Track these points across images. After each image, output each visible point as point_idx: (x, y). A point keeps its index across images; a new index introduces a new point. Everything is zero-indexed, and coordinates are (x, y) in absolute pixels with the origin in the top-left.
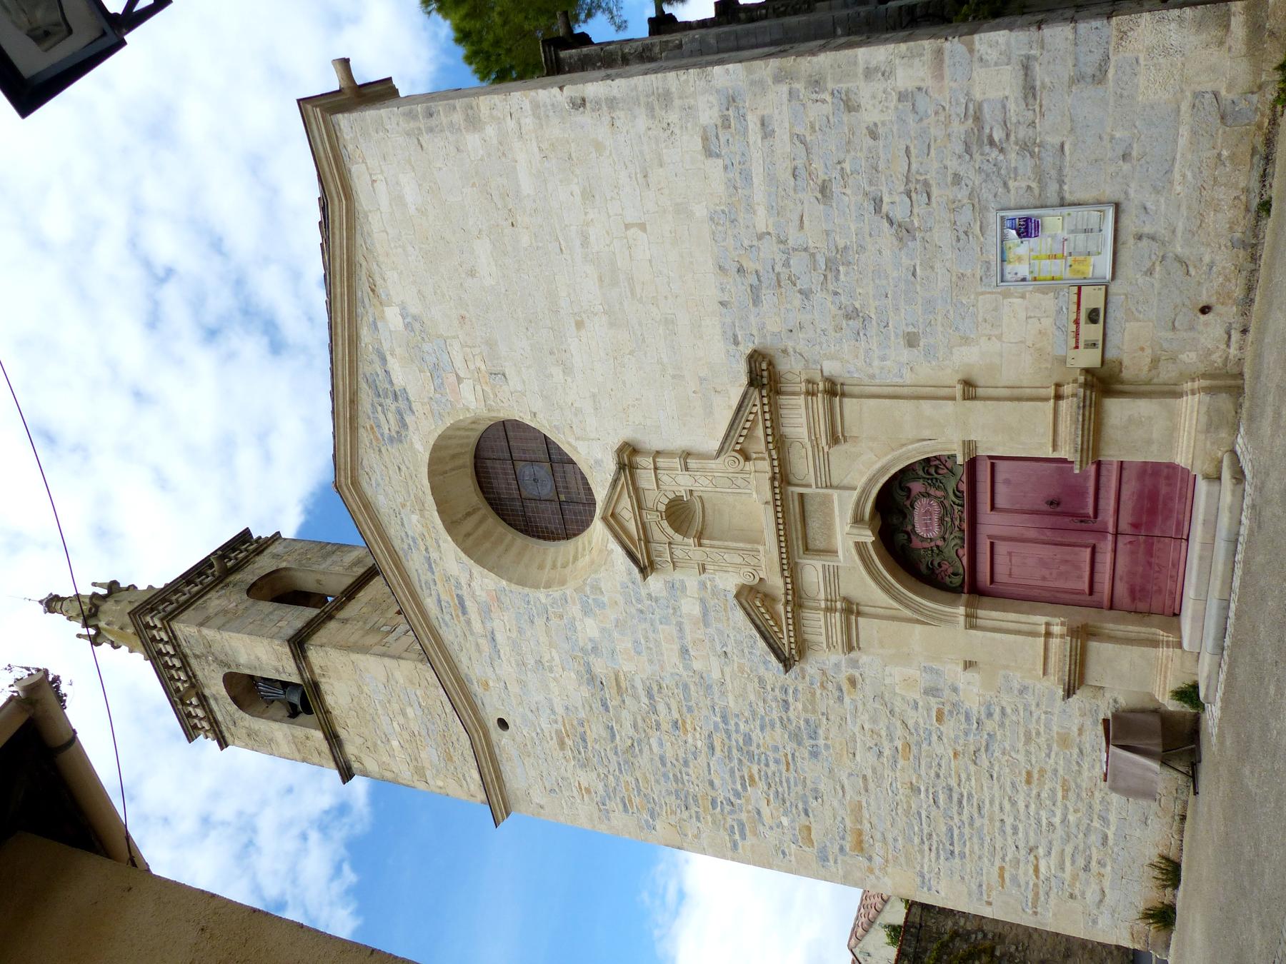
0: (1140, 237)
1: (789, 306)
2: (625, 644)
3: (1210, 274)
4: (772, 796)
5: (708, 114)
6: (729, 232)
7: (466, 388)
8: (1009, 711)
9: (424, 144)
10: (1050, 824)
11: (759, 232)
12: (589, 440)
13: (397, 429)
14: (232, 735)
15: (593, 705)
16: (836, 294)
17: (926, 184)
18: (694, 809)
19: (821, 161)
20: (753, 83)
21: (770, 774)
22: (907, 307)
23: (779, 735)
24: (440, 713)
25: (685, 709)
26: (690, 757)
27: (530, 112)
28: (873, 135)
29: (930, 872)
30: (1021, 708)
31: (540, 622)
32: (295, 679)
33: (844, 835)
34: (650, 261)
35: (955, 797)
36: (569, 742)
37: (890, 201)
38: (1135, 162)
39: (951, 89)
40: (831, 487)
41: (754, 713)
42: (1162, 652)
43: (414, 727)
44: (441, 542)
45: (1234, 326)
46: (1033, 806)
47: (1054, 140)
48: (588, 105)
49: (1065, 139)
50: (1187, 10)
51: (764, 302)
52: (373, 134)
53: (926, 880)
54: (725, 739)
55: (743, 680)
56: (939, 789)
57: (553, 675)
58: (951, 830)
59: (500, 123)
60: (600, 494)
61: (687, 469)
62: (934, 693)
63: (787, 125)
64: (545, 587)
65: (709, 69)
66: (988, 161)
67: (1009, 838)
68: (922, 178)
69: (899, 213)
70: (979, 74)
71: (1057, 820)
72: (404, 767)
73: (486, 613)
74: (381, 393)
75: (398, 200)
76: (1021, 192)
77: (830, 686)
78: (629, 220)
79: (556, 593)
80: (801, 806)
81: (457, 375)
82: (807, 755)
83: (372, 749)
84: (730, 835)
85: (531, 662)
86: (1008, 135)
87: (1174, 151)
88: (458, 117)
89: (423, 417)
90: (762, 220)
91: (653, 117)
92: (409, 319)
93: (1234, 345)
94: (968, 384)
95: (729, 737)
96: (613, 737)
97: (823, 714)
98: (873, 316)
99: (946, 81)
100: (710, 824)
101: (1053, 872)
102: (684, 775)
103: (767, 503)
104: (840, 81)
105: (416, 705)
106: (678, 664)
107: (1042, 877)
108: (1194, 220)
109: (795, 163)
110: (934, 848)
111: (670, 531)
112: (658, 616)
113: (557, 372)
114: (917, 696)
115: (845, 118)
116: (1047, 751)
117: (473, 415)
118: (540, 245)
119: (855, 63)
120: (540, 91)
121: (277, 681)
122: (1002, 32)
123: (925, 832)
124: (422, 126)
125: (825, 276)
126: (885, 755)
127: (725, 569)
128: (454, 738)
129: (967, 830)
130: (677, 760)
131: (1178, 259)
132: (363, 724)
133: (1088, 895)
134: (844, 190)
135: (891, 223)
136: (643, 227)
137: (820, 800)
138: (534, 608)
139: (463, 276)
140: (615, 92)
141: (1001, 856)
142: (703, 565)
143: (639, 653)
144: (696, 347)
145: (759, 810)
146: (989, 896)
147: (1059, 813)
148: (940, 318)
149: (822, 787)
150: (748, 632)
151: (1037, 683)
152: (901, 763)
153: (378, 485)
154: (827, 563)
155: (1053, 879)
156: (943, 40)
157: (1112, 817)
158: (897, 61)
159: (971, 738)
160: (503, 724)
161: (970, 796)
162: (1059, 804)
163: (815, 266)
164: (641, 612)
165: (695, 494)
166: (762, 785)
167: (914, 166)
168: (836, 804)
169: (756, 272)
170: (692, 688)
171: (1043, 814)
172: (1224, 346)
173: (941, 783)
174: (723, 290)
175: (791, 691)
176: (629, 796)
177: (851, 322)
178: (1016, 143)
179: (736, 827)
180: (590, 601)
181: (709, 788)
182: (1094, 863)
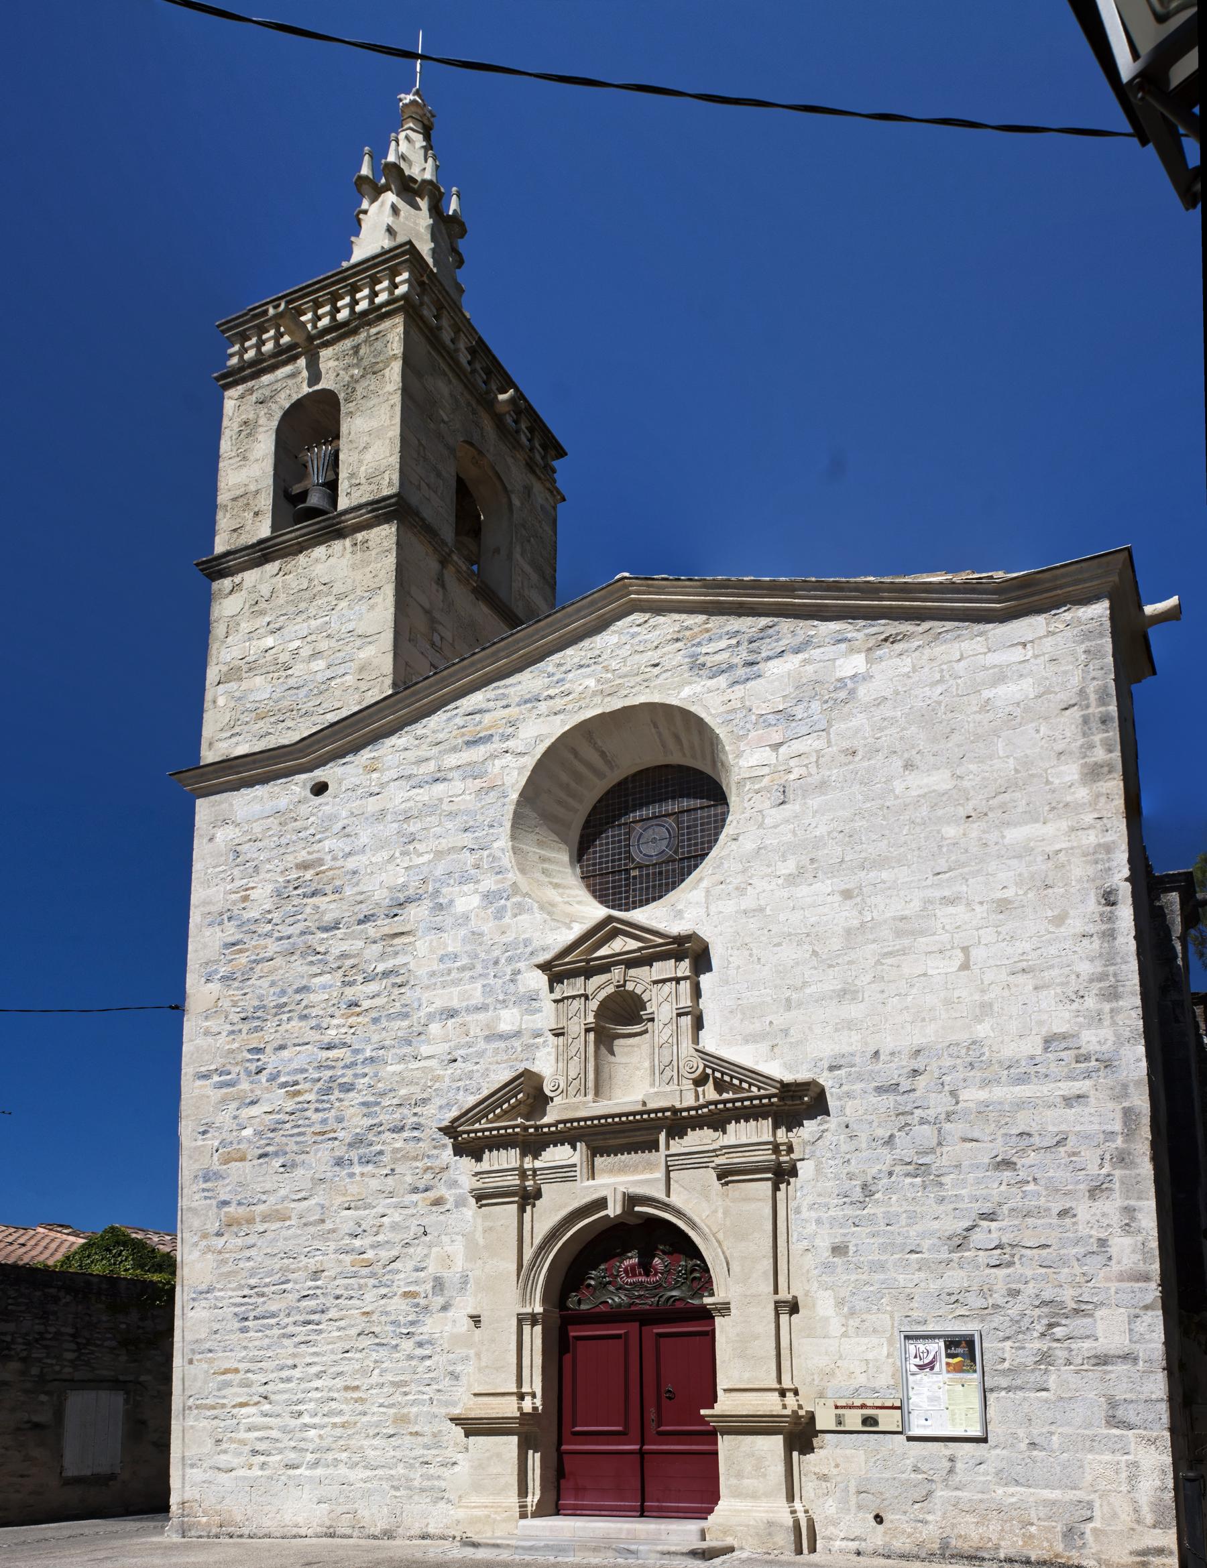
0: (951, 1460)
1: (875, 1124)
2: (452, 942)
3: (916, 1521)
4: (278, 1116)
5: (1092, 1039)
6: (959, 1061)
7: (767, 755)
8: (428, 1363)
9: (1068, 712)
10: (300, 1414)
11: (959, 1092)
12: (707, 903)
13: (709, 665)
14: (242, 397)
15: (363, 906)
16: (890, 1174)
17: (1010, 1264)
18: (245, 1027)
19: (1037, 1162)
20: (1125, 1086)
21: (308, 1114)
22: (876, 1245)
23: (358, 1122)
24: (324, 705)
25: (374, 1014)
26: (313, 1022)
27: (1102, 841)
28: (1063, 1213)
29: (216, 1298)
30: (431, 1375)
31: (467, 839)
32: (343, 503)
33: (244, 1204)
34: (925, 975)
35: (315, 1317)
36: (309, 875)
37: (992, 1228)
38: (1028, 1453)
39: (1109, 1288)
40: (668, 1172)
41: (383, 1094)
42: (513, 1499)
43: (298, 669)
44: (561, 716)
45: (863, 1544)
46: (318, 1395)
47: (1052, 1381)
48: (1109, 908)
49: (1052, 1392)
50: (1172, 1494)
51: (880, 1098)
52: (1083, 647)
53: (204, 1295)
54: (344, 1062)
55: (423, 1081)
56: (322, 1300)
57: (397, 854)
58: (273, 1316)
59: (1090, 805)
60: (640, 915)
61: (679, 1015)
62: (438, 1288)
63: (1078, 1128)
64: (513, 848)
65: (1143, 1041)
66: (1033, 1322)
67: (275, 1375)
68: (1016, 1259)
69: (977, 1237)
70: (1122, 1314)
71: (306, 1419)
72: (236, 652)
73: (473, 772)
74: (753, 644)
75: (1000, 678)
76: (1000, 1353)
77: (429, 1176)
78: (974, 952)
79: (507, 860)
80: (270, 1149)
81: (781, 744)
82: (337, 1153)
83: (256, 608)
84: (216, 1070)
85: (413, 827)
86: (1058, 1340)
87: (1037, 1486)
88: (1100, 755)
89: (726, 698)
90: (972, 1096)
91: (1091, 981)
92: (850, 685)
93: (844, 1543)
94: (794, 1308)
95: (346, 1067)
96: (326, 929)
97: (393, 1170)
98: (865, 1212)
99: (1117, 1284)
100: (227, 1047)
101: (244, 1421)
102: (288, 1015)
103: (644, 1104)
104: (1122, 1183)
105: (329, 674)
106: (434, 1005)
107: (235, 1411)
108: (968, 1505)
109: (1036, 1134)
110: (246, 1300)
111: (602, 995)
112: (492, 983)
113: (790, 867)
114: (431, 1270)
115: (1083, 1187)
116: (386, 1404)
117: (732, 763)
118: (944, 850)
119: (1139, 1198)
120: (1126, 856)
121: (337, 474)
122: (1163, 1336)
123: (265, 1290)
124: (1090, 711)
125: (910, 1163)
126: (354, 1241)
127: (560, 1058)
128: (289, 723)
129: (276, 1332)
130: (306, 1007)
131: (929, 1494)
132: (292, 598)
133: (223, 1457)
134: (1004, 1183)
135: (968, 1230)
136: (965, 966)
137: (282, 1169)
138: (485, 832)
139: (906, 755)
140: (1121, 940)
141: (252, 1369)
142: (562, 1034)
143: (441, 960)
144: (825, 1024)
145: (256, 1103)
146: (199, 1361)
147: (316, 1420)
148: (864, 1277)
149: (300, 1172)
150: (485, 1085)
151: (464, 1389)
152: (347, 1259)
153: (633, 636)
154: (578, 1169)
155: (235, 1421)
156: (1159, 1282)
157: (319, 1471)
158: (1140, 1238)
159: (390, 1328)
160: (320, 789)
161: (320, 1332)
162: (326, 1419)
163: (920, 1153)
164: (496, 963)
165: (650, 1024)
166: (290, 1105)
167: (1028, 1252)
168: (282, 1192)
169: (914, 1090)
170: (406, 1023)
171: (312, 1406)
172: (842, 1535)
173: (329, 1301)
174: (892, 1054)
175: (416, 1135)
176: (247, 950)
177: (858, 1189)
178: (1049, 1349)
179: (229, 1077)
180: (503, 901)
181: (276, 1045)
182: (262, 1458)
